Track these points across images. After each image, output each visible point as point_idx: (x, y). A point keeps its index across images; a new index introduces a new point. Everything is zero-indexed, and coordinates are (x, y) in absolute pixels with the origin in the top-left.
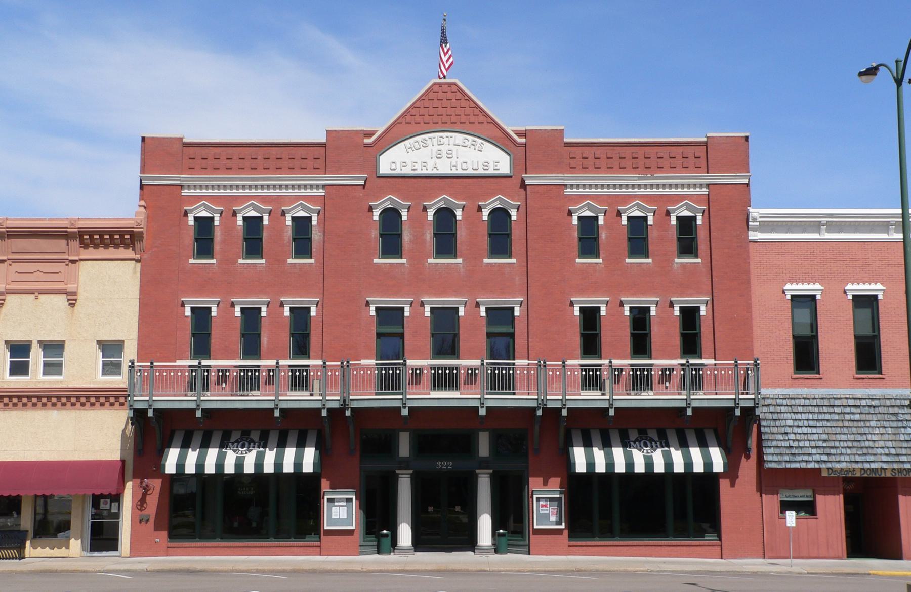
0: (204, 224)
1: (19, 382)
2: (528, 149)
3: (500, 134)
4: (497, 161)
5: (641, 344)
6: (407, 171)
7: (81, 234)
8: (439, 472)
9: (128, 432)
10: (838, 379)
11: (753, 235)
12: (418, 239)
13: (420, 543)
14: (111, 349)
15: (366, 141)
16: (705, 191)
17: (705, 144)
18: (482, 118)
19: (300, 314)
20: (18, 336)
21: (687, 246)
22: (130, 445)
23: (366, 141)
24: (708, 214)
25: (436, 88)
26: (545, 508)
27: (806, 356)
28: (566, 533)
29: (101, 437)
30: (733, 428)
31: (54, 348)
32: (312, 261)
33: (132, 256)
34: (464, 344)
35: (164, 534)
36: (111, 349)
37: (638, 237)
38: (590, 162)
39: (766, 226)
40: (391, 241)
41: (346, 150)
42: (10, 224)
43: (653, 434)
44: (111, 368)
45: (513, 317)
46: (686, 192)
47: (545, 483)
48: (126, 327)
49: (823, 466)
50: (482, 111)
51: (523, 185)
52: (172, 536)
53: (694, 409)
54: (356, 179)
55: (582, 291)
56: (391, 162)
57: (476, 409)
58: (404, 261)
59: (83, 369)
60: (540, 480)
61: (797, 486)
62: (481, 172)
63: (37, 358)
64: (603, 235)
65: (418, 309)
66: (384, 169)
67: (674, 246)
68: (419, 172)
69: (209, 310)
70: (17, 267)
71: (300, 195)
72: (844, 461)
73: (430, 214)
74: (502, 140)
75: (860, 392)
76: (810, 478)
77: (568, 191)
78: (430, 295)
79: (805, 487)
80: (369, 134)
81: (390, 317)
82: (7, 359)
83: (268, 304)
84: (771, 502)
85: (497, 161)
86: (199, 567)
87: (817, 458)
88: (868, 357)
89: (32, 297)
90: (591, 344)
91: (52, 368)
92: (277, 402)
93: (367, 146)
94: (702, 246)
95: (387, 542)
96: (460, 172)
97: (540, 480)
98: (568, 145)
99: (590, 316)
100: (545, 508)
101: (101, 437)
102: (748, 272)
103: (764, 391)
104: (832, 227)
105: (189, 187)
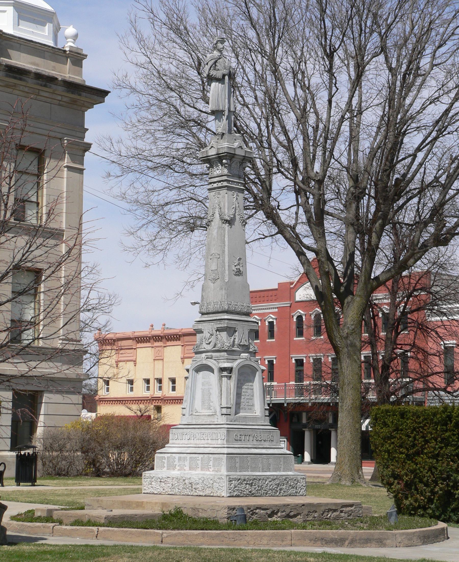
7: (153, 337)
13: (314, 461)
21: (271, 335)
23: (292, 286)
32: (274, 340)
33: (150, 345)
42: (183, 331)
53: (273, 404)
54: (286, 304)
57: (283, 404)
66: (297, 299)
69: (303, 360)
73: (313, 317)
80: (292, 283)
83: (276, 358)
89: (124, 363)
90: (299, 377)
92: (285, 400)
93: (291, 288)
95: (300, 458)
99: (300, 363)
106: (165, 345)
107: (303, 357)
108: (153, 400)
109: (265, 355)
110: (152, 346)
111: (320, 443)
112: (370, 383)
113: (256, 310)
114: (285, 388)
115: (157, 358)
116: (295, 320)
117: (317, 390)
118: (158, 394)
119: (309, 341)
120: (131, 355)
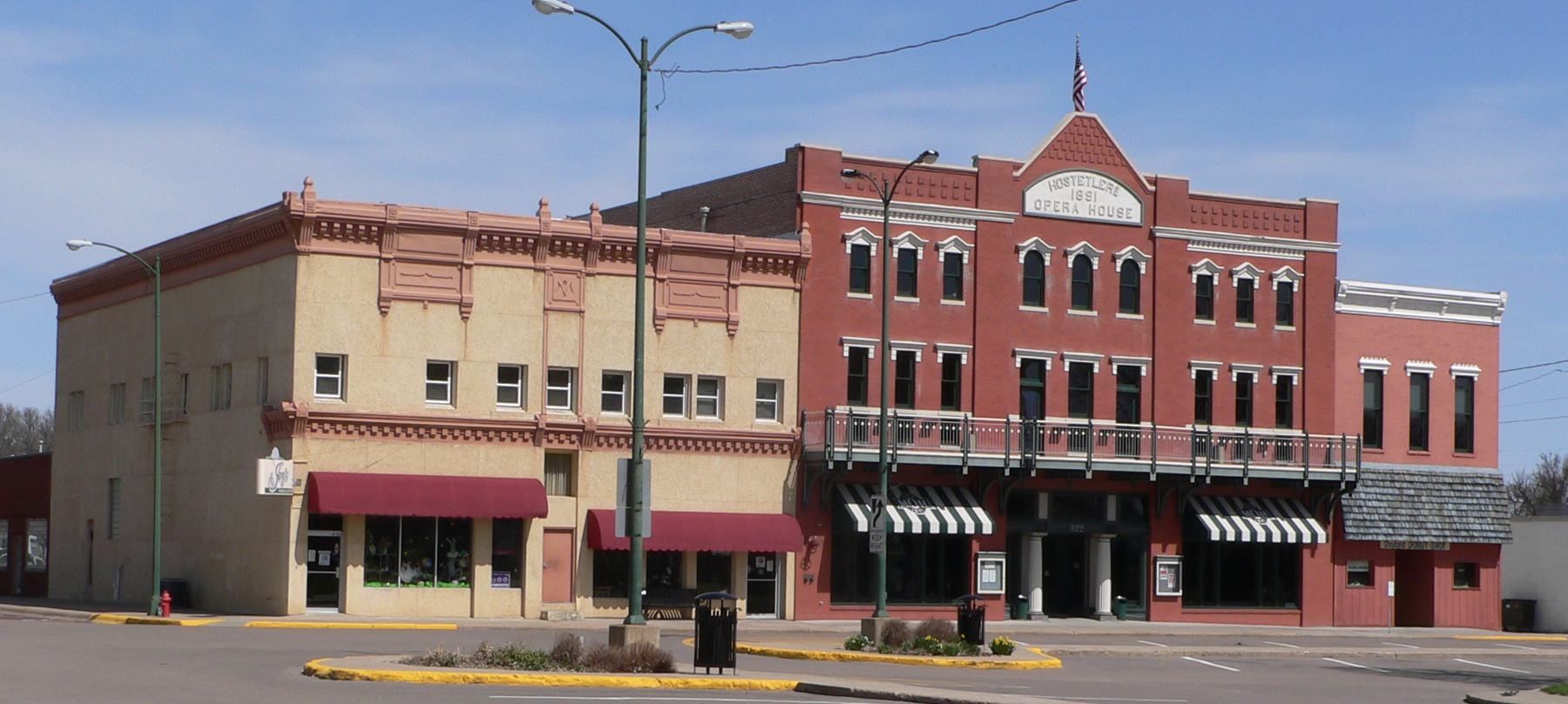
0: (861, 252)
1: (510, 411)
2: (1161, 199)
3: (1131, 178)
4: (1127, 207)
5: (1081, 402)
6: (1050, 212)
7: (553, 239)
8: (1091, 537)
9: (790, 483)
10: (1394, 459)
11: (1340, 307)
12: (1059, 286)
13: (1053, 608)
14: (768, 388)
15: (1017, 174)
16: (972, 227)
17: (1305, 208)
18: (1118, 161)
19: (951, 361)
20: (677, 369)
22: (792, 498)
23: (1017, 174)
24: (1304, 281)
25: (1078, 122)
26: (1165, 577)
27: (1373, 433)
28: (1003, 599)
29: (757, 489)
30: (1321, 499)
31: (710, 384)
33: (532, 264)
34: (1098, 404)
35: (828, 595)
36: (768, 388)
37: (908, 273)
38: (1208, 218)
39: (1352, 299)
40: (1034, 290)
41: (987, 183)
43: (914, 491)
44: (765, 410)
45: (1092, 373)
46: (1283, 255)
47: (1164, 550)
48: (784, 365)
49: (1381, 538)
50: (1118, 151)
51: (1152, 237)
52: (833, 600)
53: (1158, 475)
55: (1199, 356)
56: (1044, 197)
58: (1046, 310)
59: (740, 413)
60: (1160, 546)
61: (1357, 557)
62: (1115, 219)
63: (692, 394)
64: (1217, 296)
65: (1058, 361)
66: (1030, 208)
67: (1273, 313)
68: (1062, 214)
69: (1043, 363)
70: (401, 267)
71: (947, 228)
72: (1402, 536)
74: (1132, 183)
75: (1414, 468)
76: (1372, 552)
77: (1191, 248)
78: (1239, 361)
79: (1360, 558)
80: (1017, 167)
81: (1034, 369)
82: (424, 380)
84: (1341, 572)
85: (1127, 207)
86: (813, 628)
87: (1385, 530)
88: (1419, 437)
89: (691, 323)
90: (1203, 412)
91: (708, 407)
93: (1016, 179)
94: (1297, 315)
96: (1097, 217)
97: (1160, 546)
98: (1193, 197)
100: (1165, 577)
101: (757, 489)
102: (1333, 343)
103: (1364, 465)
104: (1403, 304)
105: (1193, 242)
106: (590, 269)
107: (963, 350)
108: (310, 422)
109: (937, 337)
110: (539, 265)
111: (1077, 566)
112: (1288, 439)
113: (901, 215)
114: (1008, 430)
115: (556, 305)
116: (1022, 261)
117: (1079, 441)
118: (561, 414)
119: (1399, 358)
120: (449, 283)
